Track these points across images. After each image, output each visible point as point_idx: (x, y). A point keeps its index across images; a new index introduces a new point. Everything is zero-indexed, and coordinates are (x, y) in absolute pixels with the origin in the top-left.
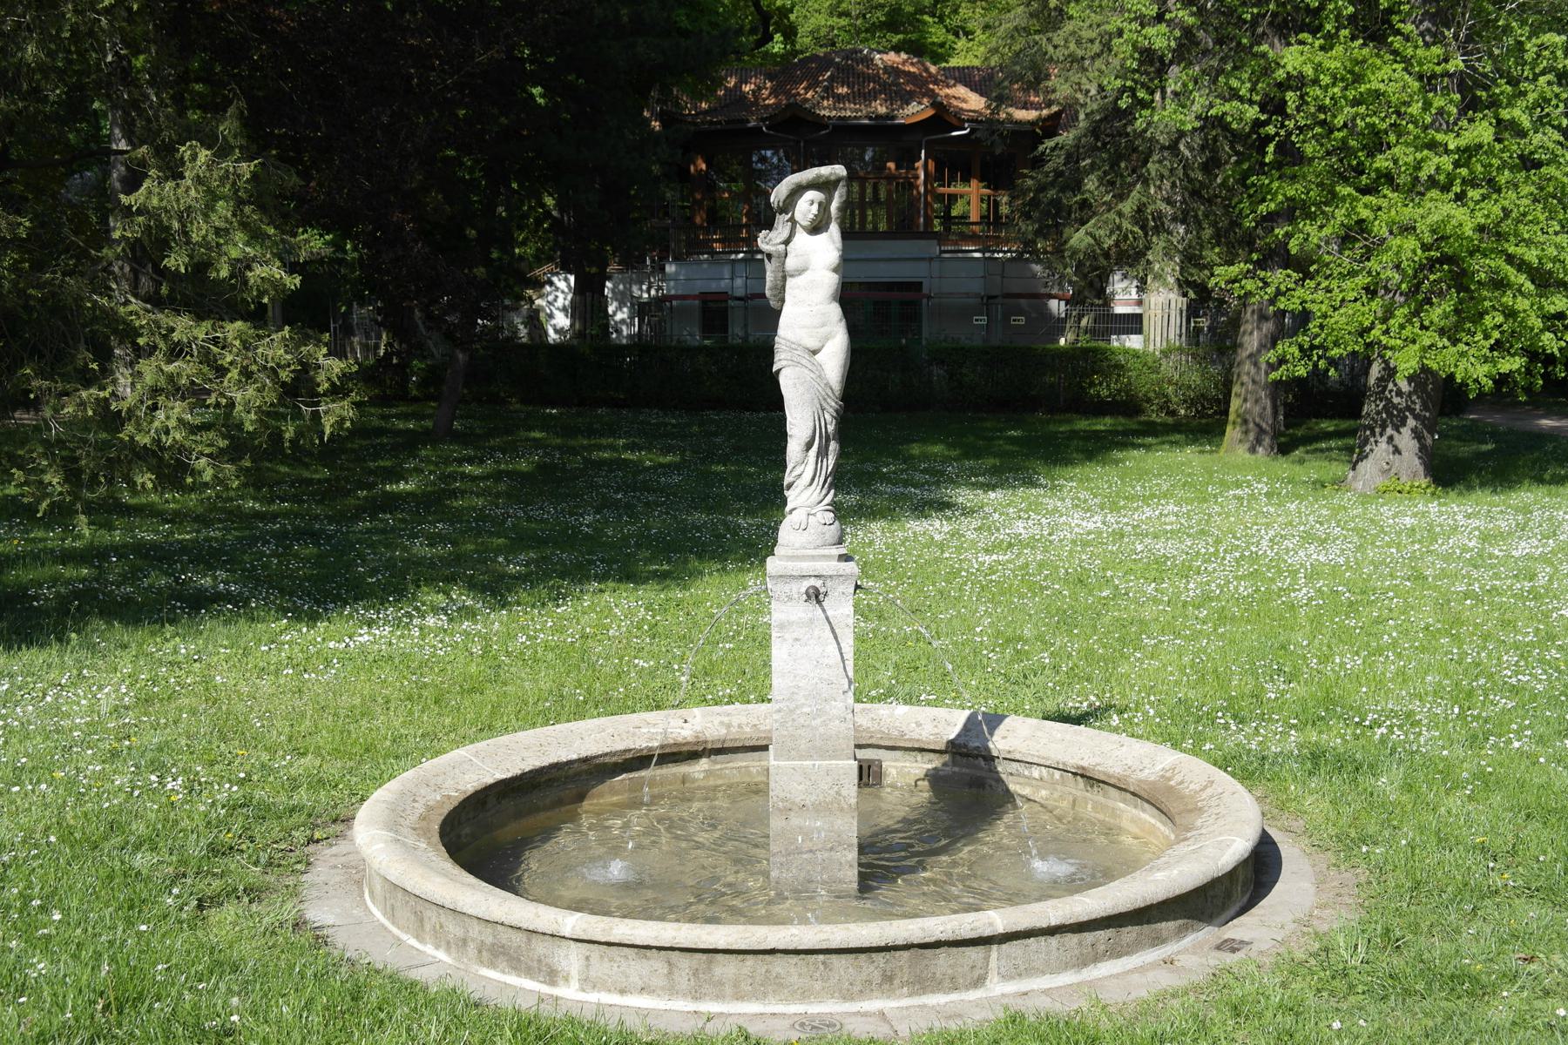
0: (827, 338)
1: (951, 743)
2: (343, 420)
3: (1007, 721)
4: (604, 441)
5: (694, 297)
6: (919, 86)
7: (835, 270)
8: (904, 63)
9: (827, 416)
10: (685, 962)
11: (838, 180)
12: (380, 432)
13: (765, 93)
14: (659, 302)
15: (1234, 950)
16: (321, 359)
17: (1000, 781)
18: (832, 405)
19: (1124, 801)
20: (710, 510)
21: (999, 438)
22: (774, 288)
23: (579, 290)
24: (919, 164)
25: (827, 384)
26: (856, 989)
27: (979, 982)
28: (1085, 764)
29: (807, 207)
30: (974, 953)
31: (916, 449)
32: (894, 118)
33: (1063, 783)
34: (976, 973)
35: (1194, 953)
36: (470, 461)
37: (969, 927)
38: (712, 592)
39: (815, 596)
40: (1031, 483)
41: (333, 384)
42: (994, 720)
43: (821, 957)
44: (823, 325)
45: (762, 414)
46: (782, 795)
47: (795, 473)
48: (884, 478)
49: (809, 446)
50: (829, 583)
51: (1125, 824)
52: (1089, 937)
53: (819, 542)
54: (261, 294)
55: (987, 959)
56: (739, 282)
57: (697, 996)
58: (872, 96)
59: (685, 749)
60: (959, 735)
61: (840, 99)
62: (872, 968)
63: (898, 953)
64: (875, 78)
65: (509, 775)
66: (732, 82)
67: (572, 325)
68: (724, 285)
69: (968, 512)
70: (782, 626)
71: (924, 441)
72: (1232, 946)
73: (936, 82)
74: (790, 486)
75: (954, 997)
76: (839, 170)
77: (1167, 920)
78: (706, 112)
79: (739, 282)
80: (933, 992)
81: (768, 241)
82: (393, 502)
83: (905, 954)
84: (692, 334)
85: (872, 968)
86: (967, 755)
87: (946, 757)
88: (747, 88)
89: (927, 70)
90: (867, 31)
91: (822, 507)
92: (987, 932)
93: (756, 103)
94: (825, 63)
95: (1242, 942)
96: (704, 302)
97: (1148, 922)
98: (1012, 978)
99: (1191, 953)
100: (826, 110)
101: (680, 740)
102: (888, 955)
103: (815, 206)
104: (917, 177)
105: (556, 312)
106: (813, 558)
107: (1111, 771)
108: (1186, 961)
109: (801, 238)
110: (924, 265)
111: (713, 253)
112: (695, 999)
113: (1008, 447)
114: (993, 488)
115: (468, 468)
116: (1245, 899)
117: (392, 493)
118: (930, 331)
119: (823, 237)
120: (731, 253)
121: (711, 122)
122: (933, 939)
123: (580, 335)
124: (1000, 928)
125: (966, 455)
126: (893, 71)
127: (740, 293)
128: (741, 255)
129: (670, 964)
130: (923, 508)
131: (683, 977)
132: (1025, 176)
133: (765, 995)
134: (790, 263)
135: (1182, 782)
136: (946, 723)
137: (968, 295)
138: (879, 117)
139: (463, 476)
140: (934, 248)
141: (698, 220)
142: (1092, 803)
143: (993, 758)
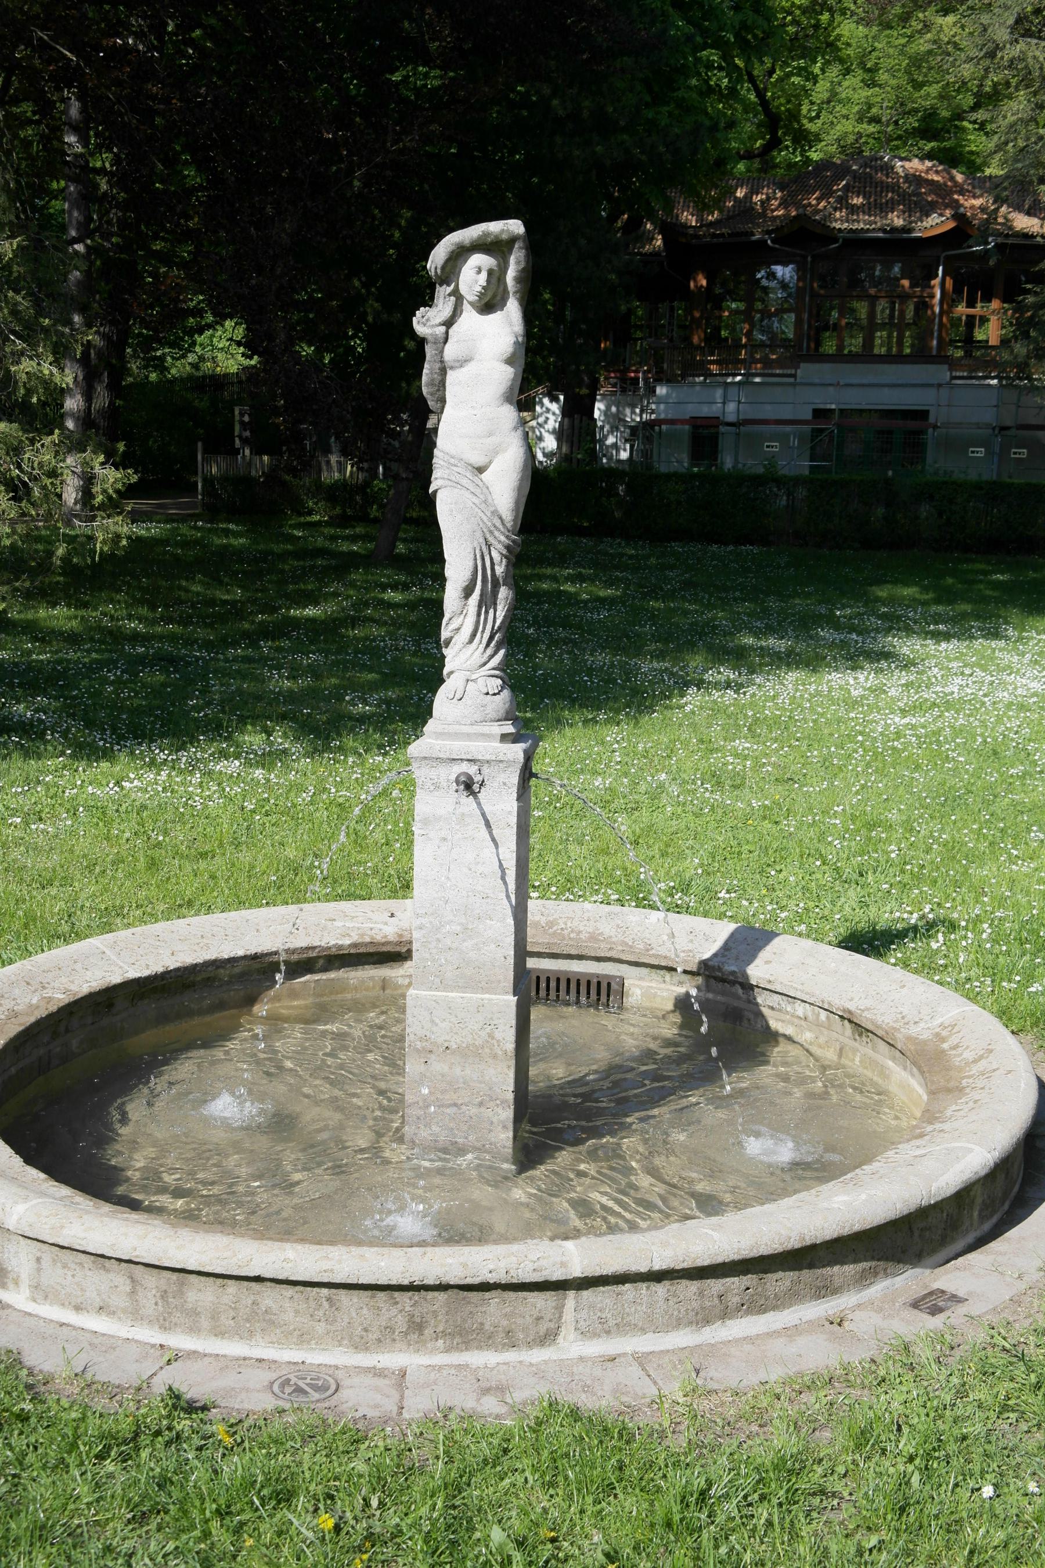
0: (496, 452)
1: (704, 964)
2: (118, 537)
3: (776, 941)
4: (549, 571)
5: (683, 422)
6: (943, 196)
7: (510, 361)
8: (929, 170)
9: (495, 555)
10: (151, 1280)
11: (512, 240)
12: (321, 552)
13: (775, 203)
14: (649, 425)
15: (935, 1311)
16: (97, 467)
17: (760, 1015)
18: (500, 542)
19: (893, 1059)
20: (617, 650)
21: (981, 581)
22: (431, 383)
23: (567, 412)
24: (936, 282)
25: (495, 513)
26: (372, 1336)
27: (548, 1338)
28: (851, 1006)
29: (473, 274)
30: (540, 1301)
31: (882, 592)
32: (910, 231)
33: (829, 1028)
34: (543, 1328)
35: (880, 1310)
36: (394, 587)
37: (531, 1266)
38: (350, 775)
39: (469, 786)
40: (995, 634)
41: (110, 498)
42: (765, 937)
43: (325, 1291)
44: (490, 435)
45: (731, 548)
46: (421, 1033)
47: (452, 627)
48: (836, 625)
49: (468, 592)
50: (486, 770)
51: (893, 1088)
52: (715, 1286)
53: (478, 717)
54: (29, 392)
55: (560, 1309)
56: (731, 407)
57: (165, 1326)
58: (884, 208)
59: (385, 949)
60: (715, 955)
61: (853, 209)
62: (396, 1311)
63: (431, 1295)
64: (894, 188)
65: (146, 973)
66: (740, 193)
67: (559, 447)
68: (714, 410)
69: (907, 665)
70: (426, 822)
71: (895, 582)
72: (932, 1303)
73: (961, 192)
74: (448, 643)
75: (511, 1356)
76: (515, 226)
77: (842, 1263)
78: (711, 224)
79: (731, 407)
80: (479, 1348)
81: (426, 322)
82: (285, 628)
83: (441, 1296)
84: (676, 460)
85: (394, 1311)
86: (723, 980)
87: (700, 980)
88: (757, 198)
89: (952, 178)
90: (899, 138)
91: (485, 671)
92: (557, 1275)
93: (763, 215)
94: (842, 171)
95: (954, 1296)
96: (695, 427)
97: (811, 1266)
98: (595, 1335)
99: (877, 1309)
100: (840, 222)
101: (379, 938)
102: (416, 1296)
103: (483, 278)
104: (933, 296)
105: (546, 435)
106: (468, 736)
107: (879, 1020)
108: (863, 1323)
109: (470, 317)
110: (932, 392)
111: (708, 374)
112: (164, 1328)
113: (988, 592)
114: (947, 637)
115: (390, 595)
116: (987, 1226)
117: (295, 618)
118: (937, 463)
119: (496, 317)
120: (728, 375)
121: (714, 235)
122: (476, 1281)
123: (567, 459)
124: (576, 1271)
125: (938, 601)
126: (915, 179)
127: (731, 418)
128: (739, 378)
129: (133, 1280)
130: (855, 657)
131: (148, 1299)
132: (1028, 292)
133: (251, 1333)
134: (450, 352)
135: (955, 1047)
136: (705, 937)
137: (978, 426)
138: (894, 230)
139: (381, 602)
140: (943, 373)
141: (696, 340)
142: (861, 1057)
143: (752, 987)
